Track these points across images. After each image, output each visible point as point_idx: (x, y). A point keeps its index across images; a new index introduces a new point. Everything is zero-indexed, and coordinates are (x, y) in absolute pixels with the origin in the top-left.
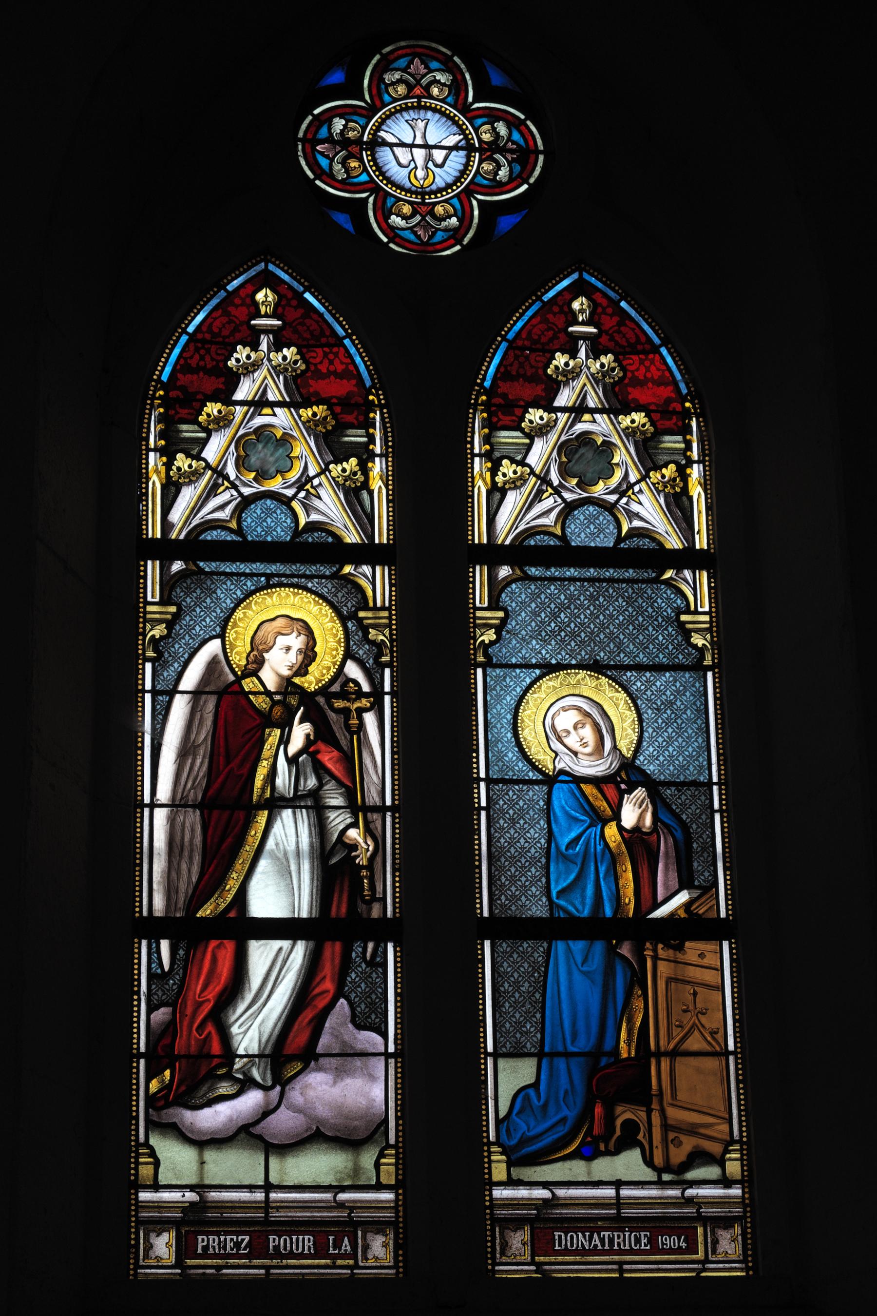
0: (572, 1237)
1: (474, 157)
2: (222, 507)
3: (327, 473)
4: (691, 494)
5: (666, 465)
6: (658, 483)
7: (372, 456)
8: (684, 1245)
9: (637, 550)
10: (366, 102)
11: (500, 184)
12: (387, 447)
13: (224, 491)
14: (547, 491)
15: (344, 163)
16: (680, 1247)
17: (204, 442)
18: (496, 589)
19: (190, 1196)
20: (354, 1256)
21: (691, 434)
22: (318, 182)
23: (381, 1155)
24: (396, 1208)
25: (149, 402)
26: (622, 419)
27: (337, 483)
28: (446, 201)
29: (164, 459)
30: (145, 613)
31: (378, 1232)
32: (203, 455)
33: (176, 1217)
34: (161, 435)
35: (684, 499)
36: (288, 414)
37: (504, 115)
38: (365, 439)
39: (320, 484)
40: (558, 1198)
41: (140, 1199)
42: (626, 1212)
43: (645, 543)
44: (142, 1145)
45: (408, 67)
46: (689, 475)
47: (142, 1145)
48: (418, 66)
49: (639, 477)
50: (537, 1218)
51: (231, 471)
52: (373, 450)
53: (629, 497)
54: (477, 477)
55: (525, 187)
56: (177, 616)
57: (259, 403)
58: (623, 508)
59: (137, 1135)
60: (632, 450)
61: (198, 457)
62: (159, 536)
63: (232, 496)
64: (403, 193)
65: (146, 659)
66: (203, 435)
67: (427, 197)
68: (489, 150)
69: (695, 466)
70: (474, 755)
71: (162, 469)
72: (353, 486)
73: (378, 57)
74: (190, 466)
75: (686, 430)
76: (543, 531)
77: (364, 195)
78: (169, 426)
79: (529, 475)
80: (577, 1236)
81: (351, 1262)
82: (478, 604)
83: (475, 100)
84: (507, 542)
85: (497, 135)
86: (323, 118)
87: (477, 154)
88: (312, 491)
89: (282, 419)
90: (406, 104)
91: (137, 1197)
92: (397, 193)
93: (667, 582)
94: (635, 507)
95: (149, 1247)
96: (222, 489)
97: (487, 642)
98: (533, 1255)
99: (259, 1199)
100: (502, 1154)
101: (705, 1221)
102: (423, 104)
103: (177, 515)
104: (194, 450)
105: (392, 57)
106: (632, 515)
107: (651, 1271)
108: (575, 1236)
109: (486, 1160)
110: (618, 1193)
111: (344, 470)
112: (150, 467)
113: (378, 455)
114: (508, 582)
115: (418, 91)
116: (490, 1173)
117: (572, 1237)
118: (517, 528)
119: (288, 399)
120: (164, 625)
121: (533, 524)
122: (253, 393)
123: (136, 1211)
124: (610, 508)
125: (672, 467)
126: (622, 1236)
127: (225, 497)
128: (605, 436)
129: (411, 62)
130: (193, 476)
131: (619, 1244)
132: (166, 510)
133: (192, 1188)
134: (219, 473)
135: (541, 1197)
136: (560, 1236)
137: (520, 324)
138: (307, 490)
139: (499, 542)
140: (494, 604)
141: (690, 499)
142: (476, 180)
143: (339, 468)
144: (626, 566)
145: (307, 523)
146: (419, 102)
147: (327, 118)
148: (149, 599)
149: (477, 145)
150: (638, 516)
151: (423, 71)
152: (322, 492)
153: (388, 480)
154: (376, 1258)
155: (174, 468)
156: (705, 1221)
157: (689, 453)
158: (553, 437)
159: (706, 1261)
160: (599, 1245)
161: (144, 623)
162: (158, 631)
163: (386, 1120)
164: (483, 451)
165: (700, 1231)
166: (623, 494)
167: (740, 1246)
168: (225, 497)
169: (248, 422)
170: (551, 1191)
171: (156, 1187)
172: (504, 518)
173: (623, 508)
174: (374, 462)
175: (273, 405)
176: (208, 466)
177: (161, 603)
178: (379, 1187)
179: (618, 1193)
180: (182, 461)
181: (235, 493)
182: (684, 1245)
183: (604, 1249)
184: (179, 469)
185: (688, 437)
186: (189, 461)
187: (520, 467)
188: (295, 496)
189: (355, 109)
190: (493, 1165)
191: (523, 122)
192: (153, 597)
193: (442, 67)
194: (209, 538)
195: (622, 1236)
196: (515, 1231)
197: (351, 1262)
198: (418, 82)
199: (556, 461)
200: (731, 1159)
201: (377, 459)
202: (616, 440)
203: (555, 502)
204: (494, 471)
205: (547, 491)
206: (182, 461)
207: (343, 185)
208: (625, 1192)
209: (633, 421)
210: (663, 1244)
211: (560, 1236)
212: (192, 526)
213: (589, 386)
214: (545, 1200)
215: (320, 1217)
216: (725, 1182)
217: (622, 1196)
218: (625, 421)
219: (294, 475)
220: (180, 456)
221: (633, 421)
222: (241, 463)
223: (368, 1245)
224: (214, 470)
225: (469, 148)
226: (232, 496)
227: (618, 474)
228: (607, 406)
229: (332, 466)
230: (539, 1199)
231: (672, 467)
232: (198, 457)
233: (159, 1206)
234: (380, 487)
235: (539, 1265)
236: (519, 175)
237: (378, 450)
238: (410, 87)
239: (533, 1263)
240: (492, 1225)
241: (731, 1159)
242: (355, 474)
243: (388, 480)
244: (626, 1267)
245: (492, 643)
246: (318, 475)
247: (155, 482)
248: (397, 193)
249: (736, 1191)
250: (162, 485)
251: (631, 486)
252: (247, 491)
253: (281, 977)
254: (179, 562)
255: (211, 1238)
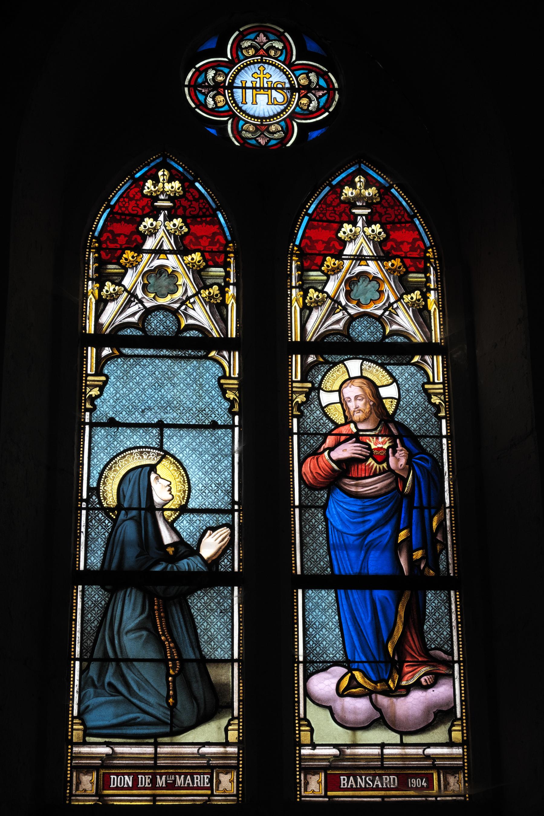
0: (121, 778)
1: (295, 95)
2: (338, 322)
3: (199, 295)
4: (430, 309)
5: (211, 286)
6: (206, 297)
7: (429, 290)
8: (425, 784)
9: (396, 344)
10: (228, 58)
11: (311, 112)
12: (438, 284)
13: (339, 312)
14: (134, 301)
15: (214, 98)
16: (422, 786)
17: (123, 275)
18: (101, 363)
19: (335, 752)
20: (211, 788)
21: (230, 267)
22: (197, 110)
23: (229, 724)
24: (238, 758)
25: (88, 250)
26: (386, 264)
27: (205, 301)
28: (277, 123)
29: (98, 285)
30: (292, 387)
31: (86, 774)
32: (123, 283)
33: (150, 763)
34: (97, 270)
35: (102, 304)
36: (376, 264)
37: (314, 69)
38: (425, 279)
39: (398, 307)
40: (116, 753)
41: (74, 752)
42: (387, 763)
43: (400, 339)
44: (302, 719)
45: (256, 38)
46: (227, 292)
47: (302, 719)
48: (262, 38)
49: (194, 292)
50: (102, 766)
51: (343, 300)
52: (429, 286)
53: (187, 305)
54: (90, 293)
55: (327, 114)
56: (312, 389)
57: (158, 252)
58: (388, 319)
59: (299, 713)
60: (191, 276)
61: (120, 284)
62: (299, 340)
63: (139, 308)
64: (250, 118)
65: (294, 416)
66: (123, 271)
67: (264, 121)
68: (218, 88)
69: (432, 292)
70: (291, 473)
71: (96, 292)
72: (216, 302)
73: (237, 33)
74: (114, 290)
75: (426, 271)
76: (336, 332)
77: (226, 119)
78: (101, 263)
79: (327, 298)
80: (124, 778)
81: (209, 792)
82: (294, 379)
83: (226, 56)
84: (313, 340)
85: (310, 82)
86: (201, 69)
87: (297, 94)
88: (393, 311)
89: (372, 268)
90: (253, 60)
91: (300, 752)
92: (246, 118)
93: (415, 364)
94: (191, 312)
95: (79, 783)
96: (338, 310)
97: (94, 396)
98: (326, 791)
99: (419, 753)
100: (81, 724)
101: (439, 769)
102: (264, 61)
103: (105, 319)
104: (118, 279)
105: (245, 33)
106: (187, 316)
107: (141, 801)
108: (122, 777)
109: (241, 731)
110: (156, 750)
111: (412, 298)
112: (293, 297)
113: (432, 289)
114: (109, 358)
115: (261, 52)
116: (299, 737)
117: (121, 778)
118: (113, 324)
119: (375, 255)
120: (98, 388)
121: (330, 328)
122: (156, 244)
123: (300, 761)
124: (175, 312)
125: (216, 287)
126: (388, 779)
127: (339, 315)
128: (174, 268)
129: (258, 35)
130: (319, 304)
131: (197, 782)
132: (98, 316)
133: (335, 746)
134: (335, 301)
135: (333, 754)
136: (114, 778)
137: (404, 203)
138: (390, 311)
139: (308, 340)
140: (99, 372)
141: (429, 312)
142: (296, 110)
143: (409, 297)
144: (149, 347)
145: (186, 325)
146: (262, 59)
147: (204, 70)
148: (89, 372)
149: (297, 87)
150: (192, 317)
151: (264, 39)
152: (399, 312)
153: (439, 304)
154: (314, 791)
155: (308, 298)
156: (439, 769)
157: (227, 279)
158: (340, 275)
159: (212, 795)
160: (354, 785)
161: (292, 394)
162: (301, 399)
163: (455, 707)
164: (94, 277)
165: (435, 776)
166: (183, 303)
167: (323, 787)
168: (340, 315)
169: (151, 262)
170: (112, 748)
171: (314, 746)
172: (311, 326)
173: (388, 319)
174: (229, 288)
175: (165, 252)
176: (126, 290)
177: (301, 381)
178: (226, 744)
179: (156, 750)
180: (109, 287)
181: (141, 306)
182: (425, 784)
183: (357, 788)
184: (311, 298)
185: (228, 269)
186: (317, 293)
187: (321, 294)
188: (179, 308)
189: (220, 63)
190: (302, 733)
191: (326, 73)
192: (296, 378)
193: (277, 39)
194: (188, 335)
195: (388, 779)
196: (314, 775)
197: (209, 792)
198: (262, 47)
199: (343, 290)
200: (455, 730)
201: (231, 287)
202: (180, 270)
203: (343, 315)
204: (100, 289)
205: (134, 301)
206: (109, 287)
207: (212, 112)
208: (386, 751)
209: (193, 259)
210: (411, 783)
211: (114, 778)
212: (319, 333)
213: (364, 242)
214: (107, 755)
215: (449, 764)
216: (450, 744)
217: (384, 753)
218: (188, 259)
219: (178, 295)
220: (108, 283)
221: (193, 259)
222: (145, 288)
223: (308, 782)
224: (332, 299)
225: (292, 89)
226: (139, 308)
227: (181, 290)
228: (175, 249)
229: (405, 296)
230: (103, 754)
231: (216, 287)
232: (120, 284)
233: (312, 758)
234: (233, 303)
235: (330, 797)
236: (323, 107)
237: (432, 287)
238: (257, 50)
239: (326, 796)
240: (300, 771)
241: (455, 730)
242: (419, 300)
243: (439, 304)
244: (158, 798)
245: (303, 403)
246: (396, 302)
247: (91, 301)
248: (246, 118)
249: (233, 750)
250: (96, 301)
251: (188, 298)
252: (148, 305)
253: (115, 610)
254: (312, 356)
255: (392, 777)
